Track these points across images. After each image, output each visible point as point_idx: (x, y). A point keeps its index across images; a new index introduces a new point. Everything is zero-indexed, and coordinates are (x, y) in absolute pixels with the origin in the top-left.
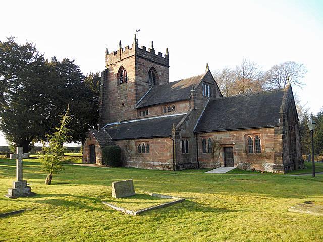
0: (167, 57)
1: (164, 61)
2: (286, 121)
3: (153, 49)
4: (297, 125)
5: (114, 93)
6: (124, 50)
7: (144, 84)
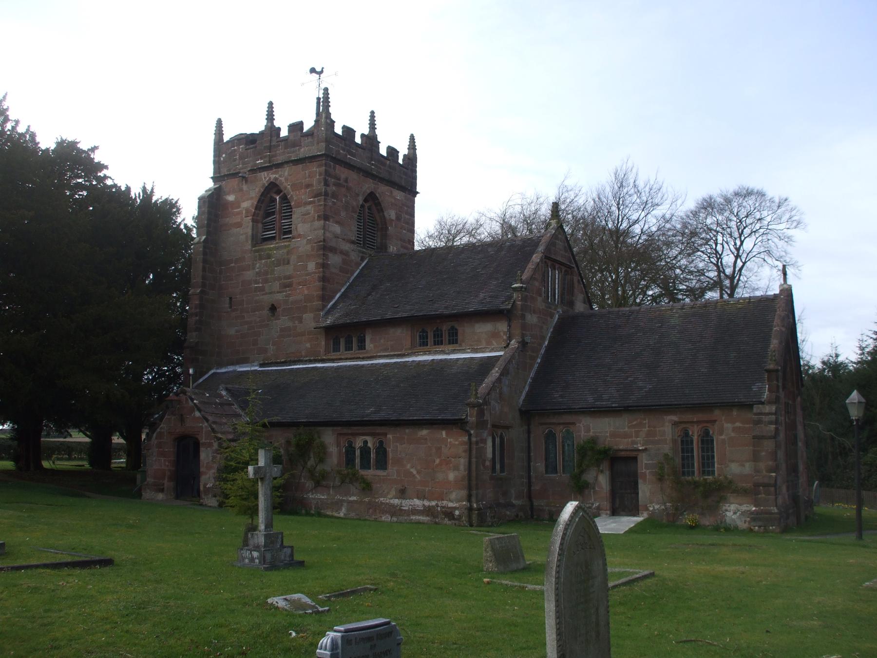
0: (411, 159)
2: (781, 390)
7: (346, 247)
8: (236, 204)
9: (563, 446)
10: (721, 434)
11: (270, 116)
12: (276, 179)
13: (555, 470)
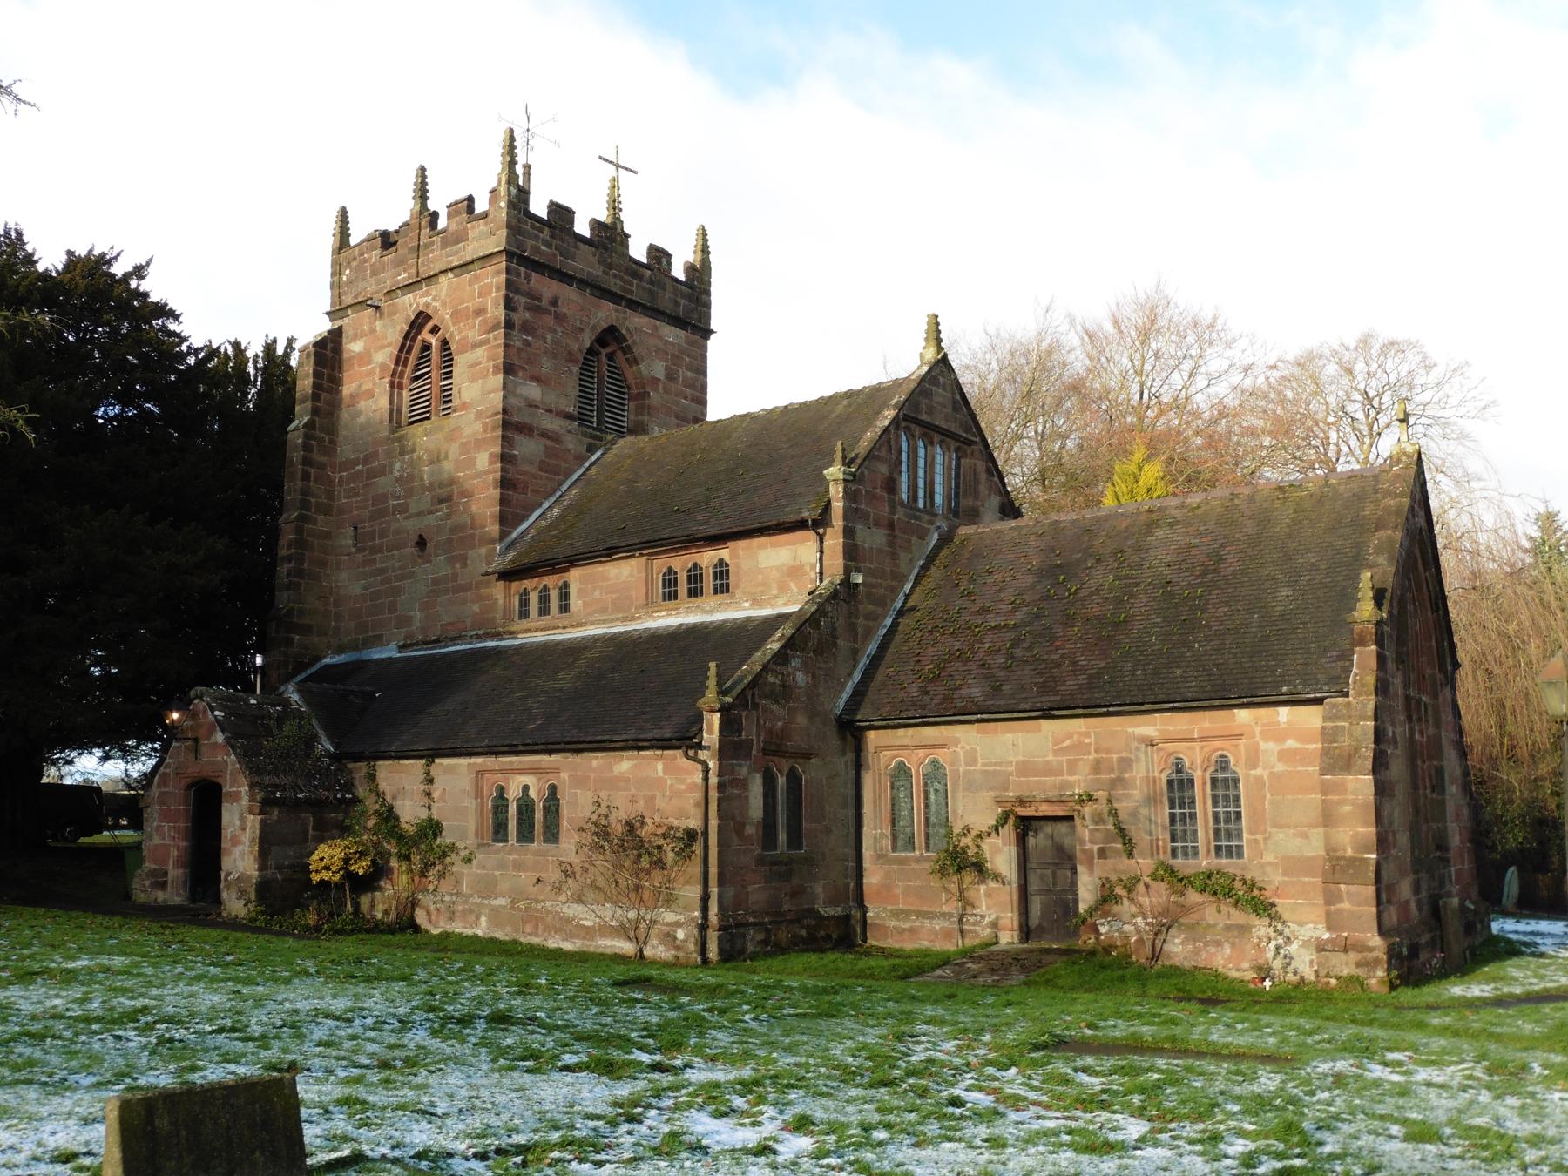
0: (700, 274)
1: (682, 302)
3: (617, 220)
4: (1447, 691)
5: (373, 474)
6: (442, 223)
8: (365, 357)
9: (926, 797)
10: (1255, 767)
11: (422, 193)
12: (427, 305)
13: (910, 843)
